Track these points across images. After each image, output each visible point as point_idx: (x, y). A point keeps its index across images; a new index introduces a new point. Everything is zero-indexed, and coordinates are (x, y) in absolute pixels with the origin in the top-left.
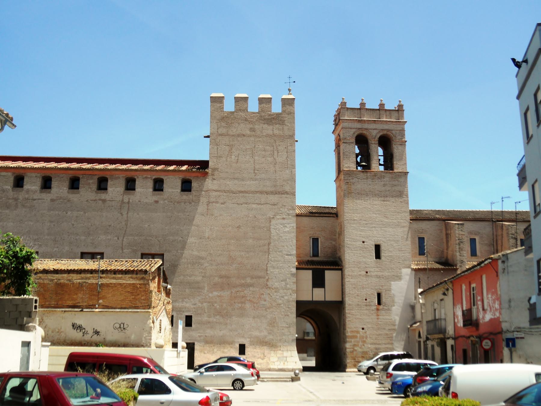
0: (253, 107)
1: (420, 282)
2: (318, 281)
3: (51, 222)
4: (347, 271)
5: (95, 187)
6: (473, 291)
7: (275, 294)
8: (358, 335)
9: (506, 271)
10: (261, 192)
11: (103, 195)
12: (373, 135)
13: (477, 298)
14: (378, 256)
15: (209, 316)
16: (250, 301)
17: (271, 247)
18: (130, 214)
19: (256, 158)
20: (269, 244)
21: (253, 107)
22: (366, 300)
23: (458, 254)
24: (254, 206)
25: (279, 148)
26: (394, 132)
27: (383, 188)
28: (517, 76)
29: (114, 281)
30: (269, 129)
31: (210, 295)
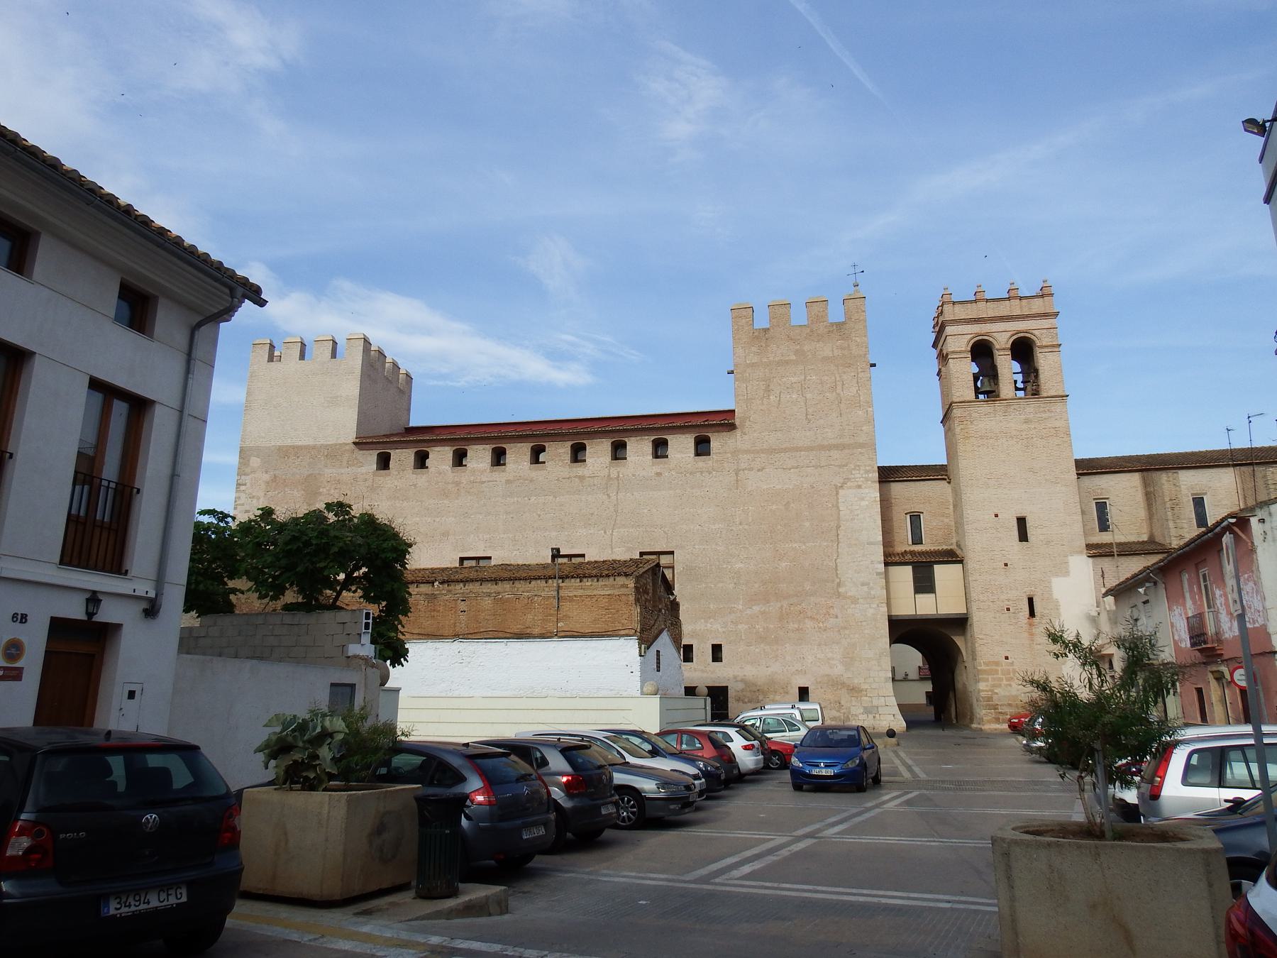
0: (799, 317)
1: (1103, 576)
2: (924, 584)
3: (507, 513)
4: (971, 564)
5: (568, 457)
6: (1205, 580)
9: (1269, 537)
10: (822, 448)
11: (579, 469)
12: (1002, 337)
13: (1214, 594)
14: (1023, 536)
15: (749, 645)
16: (812, 618)
17: (841, 533)
18: (621, 495)
19: (809, 396)
20: (838, 527)
21: (799, 317)
23: (1171, 524)
24: (809, 470)
25: (845, 377)
26: (1036, 332)
27: (1025, 426)
28: (1261, 160)
29: (580, 592)
30: (826, 349)
31: (749, 612)
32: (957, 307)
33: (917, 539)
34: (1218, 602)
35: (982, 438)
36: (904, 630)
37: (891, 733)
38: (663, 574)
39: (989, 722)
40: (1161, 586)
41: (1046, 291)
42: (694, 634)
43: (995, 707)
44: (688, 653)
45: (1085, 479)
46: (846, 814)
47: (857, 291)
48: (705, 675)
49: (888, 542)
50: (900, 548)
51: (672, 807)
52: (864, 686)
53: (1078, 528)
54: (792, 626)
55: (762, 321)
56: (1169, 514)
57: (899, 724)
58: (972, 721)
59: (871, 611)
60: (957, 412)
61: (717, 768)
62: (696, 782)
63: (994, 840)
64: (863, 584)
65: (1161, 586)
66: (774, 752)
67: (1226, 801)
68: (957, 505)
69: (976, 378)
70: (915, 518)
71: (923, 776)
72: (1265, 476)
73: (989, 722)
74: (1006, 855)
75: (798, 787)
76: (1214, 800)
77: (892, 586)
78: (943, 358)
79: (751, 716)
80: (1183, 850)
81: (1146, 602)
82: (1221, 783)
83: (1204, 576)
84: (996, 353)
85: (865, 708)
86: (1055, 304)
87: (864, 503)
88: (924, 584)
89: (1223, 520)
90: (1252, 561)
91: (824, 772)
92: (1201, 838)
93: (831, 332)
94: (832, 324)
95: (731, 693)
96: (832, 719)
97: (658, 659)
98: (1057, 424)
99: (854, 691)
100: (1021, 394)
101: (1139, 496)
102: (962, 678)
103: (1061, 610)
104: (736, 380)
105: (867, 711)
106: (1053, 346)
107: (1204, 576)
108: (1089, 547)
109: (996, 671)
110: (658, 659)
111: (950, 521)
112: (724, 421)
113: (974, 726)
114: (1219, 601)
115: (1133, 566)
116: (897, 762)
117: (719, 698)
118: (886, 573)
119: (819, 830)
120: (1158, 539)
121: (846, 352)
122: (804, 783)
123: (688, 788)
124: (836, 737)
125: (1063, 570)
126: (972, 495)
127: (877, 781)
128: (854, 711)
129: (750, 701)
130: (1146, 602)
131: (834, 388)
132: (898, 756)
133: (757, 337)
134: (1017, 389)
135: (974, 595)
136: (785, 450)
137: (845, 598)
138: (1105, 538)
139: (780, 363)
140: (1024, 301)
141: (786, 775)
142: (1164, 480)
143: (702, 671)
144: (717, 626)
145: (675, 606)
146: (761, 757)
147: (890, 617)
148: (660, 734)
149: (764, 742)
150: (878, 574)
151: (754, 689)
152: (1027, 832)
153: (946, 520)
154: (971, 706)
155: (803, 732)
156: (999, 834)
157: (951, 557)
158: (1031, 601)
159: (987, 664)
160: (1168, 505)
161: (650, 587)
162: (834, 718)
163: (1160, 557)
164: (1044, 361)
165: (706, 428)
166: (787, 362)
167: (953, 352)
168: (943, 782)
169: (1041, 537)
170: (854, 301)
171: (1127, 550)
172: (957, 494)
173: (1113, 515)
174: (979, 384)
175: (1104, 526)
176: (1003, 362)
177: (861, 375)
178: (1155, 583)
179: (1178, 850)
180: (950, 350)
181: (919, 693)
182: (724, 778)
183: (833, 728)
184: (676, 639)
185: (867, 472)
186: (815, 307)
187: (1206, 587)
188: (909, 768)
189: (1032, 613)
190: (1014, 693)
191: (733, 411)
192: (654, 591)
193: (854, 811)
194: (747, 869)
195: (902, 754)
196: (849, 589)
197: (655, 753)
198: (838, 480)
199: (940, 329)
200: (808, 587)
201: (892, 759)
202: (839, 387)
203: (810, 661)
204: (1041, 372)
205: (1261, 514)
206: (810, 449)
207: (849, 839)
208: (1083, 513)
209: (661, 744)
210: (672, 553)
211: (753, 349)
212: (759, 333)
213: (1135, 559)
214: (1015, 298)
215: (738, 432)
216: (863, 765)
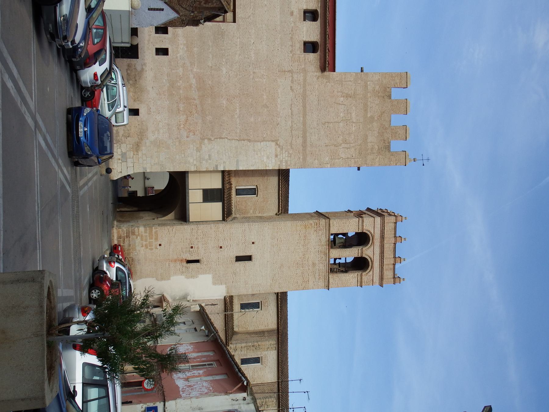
0: (397, 120)
2: (209, 196)
6: (208, 365)
7: (195, 148)
8: (153, 240)
10: (305, 132)
11: (299, 47)
12: (370, 252)
14: (239, 259)
16: (187, 120)
20: (249, 141)
21: (397, 120)
22: (192, 247)
23: (243, 345)
24: (289, 123)
26: (371, 273)
27: (311, 263)
30: (372, 139)
31: (191, 76)
32: (392, 225)
33: (239, 192)
34: (195, 372)
35: (305, 236)
36: (178, 181)
37: (109, 171)
38: (218, 16)
39: (118, 232)
40: (205, 339)
41: (397, 280)
42: (175, 36)
43: (128, 236)
44: (162, 30)
45: (275, 296)
46: (52, 146)
47: (410, 161)
48: (146, 42)
49: (238, 173)
50: (234, 181)
51: (51, 26)
52: (140, 153)
53: (243, 291)
54: (181, 106)
55: (396, 94)
56: (250, 344)
57: (116, 175)
58: (119, 221)
59: (191, 161)
60: (323, 221)
61: (80, 56)
62: (70, 43)
63: (42, 272)
64: (210, 156)
65: (205, 339)
66: (93, 93)
67: (74, 387)
68: (261, 219)
69: (345, 234)
70: (253, 192)
71: (81, 193)
72: (271, 397)
73: (118, 232)
74: (33, 280)
75: (69, 111)
76: (75, 380)
77: (209, 175)
78: (360, 214)
79: (118, 77)
80: (44, 386)
81: (195, 329)
82: (86, 384)
83: (212, 364)
84: (360, 248)
85: (125, 153)
86: (388, 285)
87: (265, 159)
88: (209, 196)
89: (246, 378)
90: (220, 392)
91: (81, 130)
92: (51, 391)
93: (385, 140)
94: (389, 143)
95: (133, 61)
96: (117, 131)
97: (157, 10)
98: (311, 283)
99: (137, 147)
100: (332, 261)
101: (262, 328)
102: (147, 216)
103: (191, 279)
104: (357, 74)
105: (124, 155)
106: (361, 282)
107: (212, 364)
108: (231, 297)
109: (152, 239)
110: (157, 10)
111: (251, 214)
112: (328, 64)
113: (115, 223)
114: (196, 372)
115: (218, 323)
116: (90, 175)
117: (132, 52)
118: (217, 171)
119: (40, 130)
120: (234, 336)
121: (369, 151)
122: (73, 116)
123: (65, 38)
124: (105, 139)
125: (217, 281)
126: (267, 229)
127: (76, 164)
128: (123, 146)
129: (128, 74)
130: (195, 329)
131: (345, 141)
132: (93, 176)
133: (385, 90)
134: (335, 259)
135: (201, 227)
136: (304, 107)
137: (201, 143)
138: (237, 307)
139: (366, 105)
140: (392, 266)
141: (77, 104)
142: (272, 342)
143: (149, 40)
144: (181, 53)
145: (195, 23)
146: (89, 85)
147: (188, 172)
148: (102, 11)
149: (101, 87)
150: (217, 166)
151: (137, 78)
152: (49, 288)
153: (251, 211)
154: (129, 221)
155: (107, 113)
156: (47, 275)
157: (227, 214)
158: (197, 261)
159: (156, 232)
160: (255, 343)
161: (210, 5)
162: (118, 132)
163: (224, 340)
164: (352, 277)
165: (323, 50)
166: (366, 111)
167: (363, 221)
168: (78, 207)
169: (238, 270)
170: (404, 158)
171: (228, 320)
172: (269, 219)
173: (251, 313)
174: (340, 236)
175: (244, 306)
176: (354, 252)
177: (353, 161)
178: (207, 336)
179: (43, 383)
180: (365, 219)
181: (137, 187)
182: (74, 60)
183: (111, 132)
184: (173, 23)
185: (286, 162)
186: (402, 132)
187: (205, 365)
188: (86, 184)
189: (189, 262)
190: (138, 248)
191: (334, 71)
192: (207, 9)
193: (56, 153)
194: (10, 84)
195: (95, 178)
196: (206, 147)
197: (89, 10)
198: (281, 142)
199: (379, 213)
200: (209, 118)
201: (91, 175)
202: (346, 146)
203: (158, 116)
204: (345, 274)
205: (249, 399)
206: (304, 124)
207: (36, 152)
208: (253, 295)
209: (95, 15)
210: (234, 21)
211: (377, 88)
212: (388, 93)
213: (223, 324)
214: (395, 261)
215: (319, 74)
216: (87, 157)
